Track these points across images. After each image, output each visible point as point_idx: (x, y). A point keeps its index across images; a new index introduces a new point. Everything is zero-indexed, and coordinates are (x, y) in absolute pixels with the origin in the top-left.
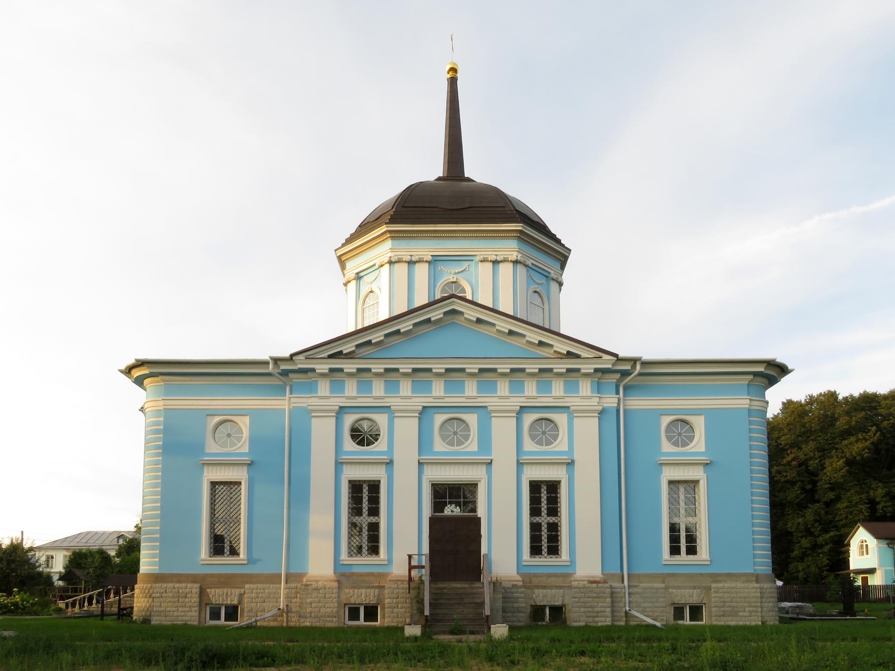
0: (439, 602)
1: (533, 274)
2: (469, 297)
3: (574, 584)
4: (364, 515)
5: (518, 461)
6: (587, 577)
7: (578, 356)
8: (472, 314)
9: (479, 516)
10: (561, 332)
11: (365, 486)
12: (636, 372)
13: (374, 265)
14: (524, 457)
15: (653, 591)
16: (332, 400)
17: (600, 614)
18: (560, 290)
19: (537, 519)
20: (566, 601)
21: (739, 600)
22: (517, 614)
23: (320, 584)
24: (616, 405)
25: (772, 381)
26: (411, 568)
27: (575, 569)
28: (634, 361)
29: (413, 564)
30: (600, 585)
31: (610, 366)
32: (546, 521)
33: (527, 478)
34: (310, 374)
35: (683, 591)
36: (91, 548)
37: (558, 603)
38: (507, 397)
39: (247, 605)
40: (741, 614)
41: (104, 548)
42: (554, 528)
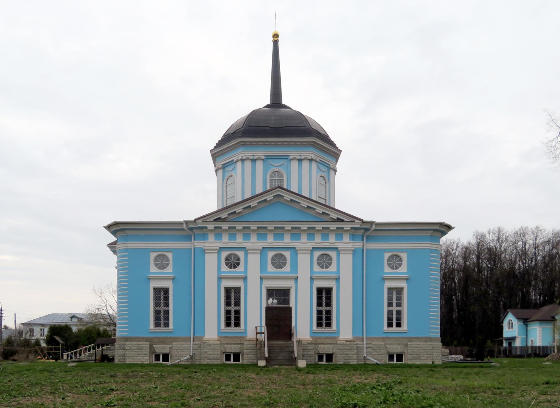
0: (272, 351)
1: (320, 165)
2: (285, 187)
3: (339, 342)
5: (311, 277)
6: (345, 339)
7: (343, 221)
8: (288, 197)
9: (291, 306)
10: (335, 208)
11: (233, 290)
12: (373, 229)
13: (233, 160)
14: (314, 275)
15: (378, 346)
16: (216, 244)
17: (351, 358)
18: (335, 174)
20: (334, 351)
21: (421, 351)
22: (310, 358)
23: (211, 342)
24: (361, 247)
25: (444, 233)
26: (257, 333)
27: (339, 335)
28: (372, 223)
29: (257, 332)
30: (351, 343)
31: (359, 226)
32: (325, 309)
33: (316, 286)
34: (204, 230)
35: (393, 346)
36: (61, 324)
37: (330, 352)
38: (306, 243)
39: (174, 353)
40: (422, 358)
41: (68, 324)
42: (329, 313)
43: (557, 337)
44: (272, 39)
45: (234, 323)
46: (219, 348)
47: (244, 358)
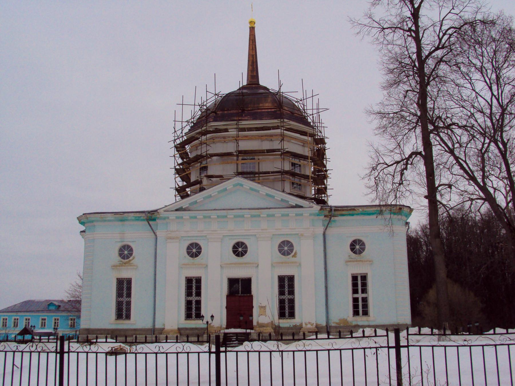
4: (193, 296)
7: (302, 207)
44: (249, 26)
45: (195, 314)
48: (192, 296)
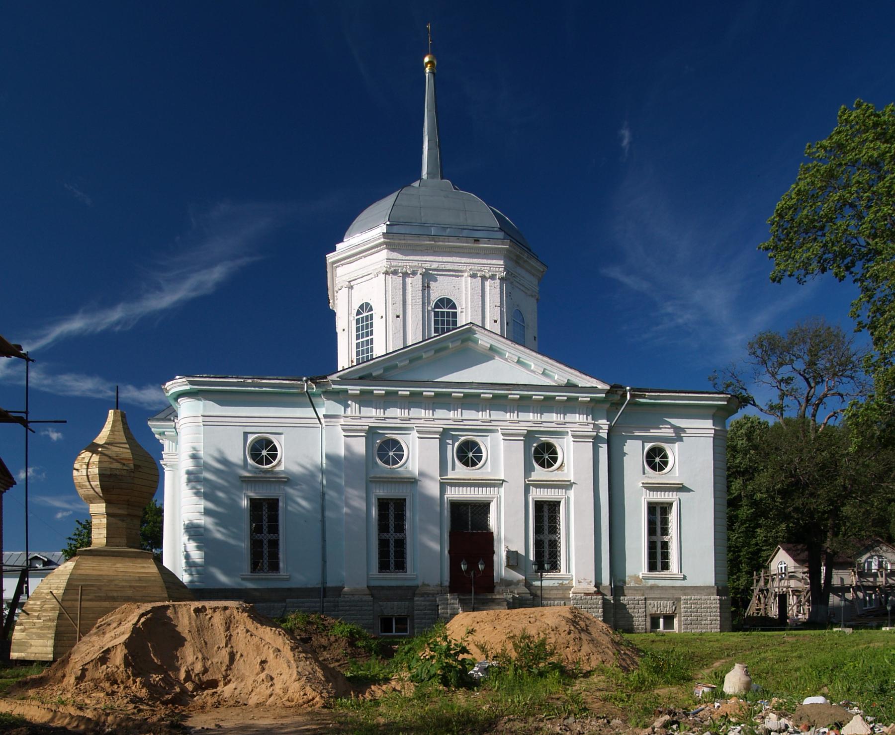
19: (385, 536)
43: (10, 586)
46: (371, 608)
47: (416, 626)
48: (395, 532)
